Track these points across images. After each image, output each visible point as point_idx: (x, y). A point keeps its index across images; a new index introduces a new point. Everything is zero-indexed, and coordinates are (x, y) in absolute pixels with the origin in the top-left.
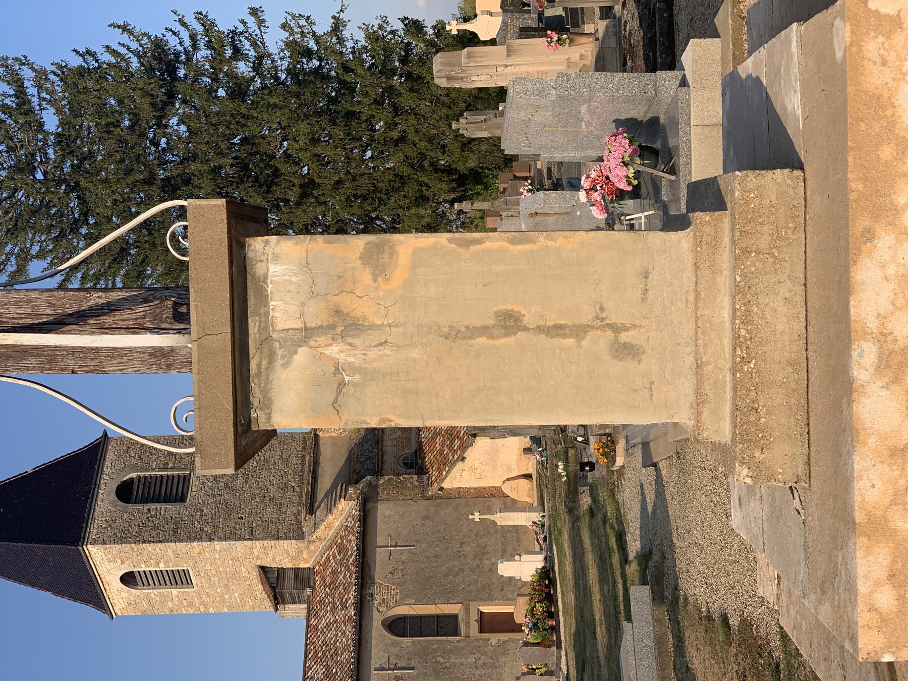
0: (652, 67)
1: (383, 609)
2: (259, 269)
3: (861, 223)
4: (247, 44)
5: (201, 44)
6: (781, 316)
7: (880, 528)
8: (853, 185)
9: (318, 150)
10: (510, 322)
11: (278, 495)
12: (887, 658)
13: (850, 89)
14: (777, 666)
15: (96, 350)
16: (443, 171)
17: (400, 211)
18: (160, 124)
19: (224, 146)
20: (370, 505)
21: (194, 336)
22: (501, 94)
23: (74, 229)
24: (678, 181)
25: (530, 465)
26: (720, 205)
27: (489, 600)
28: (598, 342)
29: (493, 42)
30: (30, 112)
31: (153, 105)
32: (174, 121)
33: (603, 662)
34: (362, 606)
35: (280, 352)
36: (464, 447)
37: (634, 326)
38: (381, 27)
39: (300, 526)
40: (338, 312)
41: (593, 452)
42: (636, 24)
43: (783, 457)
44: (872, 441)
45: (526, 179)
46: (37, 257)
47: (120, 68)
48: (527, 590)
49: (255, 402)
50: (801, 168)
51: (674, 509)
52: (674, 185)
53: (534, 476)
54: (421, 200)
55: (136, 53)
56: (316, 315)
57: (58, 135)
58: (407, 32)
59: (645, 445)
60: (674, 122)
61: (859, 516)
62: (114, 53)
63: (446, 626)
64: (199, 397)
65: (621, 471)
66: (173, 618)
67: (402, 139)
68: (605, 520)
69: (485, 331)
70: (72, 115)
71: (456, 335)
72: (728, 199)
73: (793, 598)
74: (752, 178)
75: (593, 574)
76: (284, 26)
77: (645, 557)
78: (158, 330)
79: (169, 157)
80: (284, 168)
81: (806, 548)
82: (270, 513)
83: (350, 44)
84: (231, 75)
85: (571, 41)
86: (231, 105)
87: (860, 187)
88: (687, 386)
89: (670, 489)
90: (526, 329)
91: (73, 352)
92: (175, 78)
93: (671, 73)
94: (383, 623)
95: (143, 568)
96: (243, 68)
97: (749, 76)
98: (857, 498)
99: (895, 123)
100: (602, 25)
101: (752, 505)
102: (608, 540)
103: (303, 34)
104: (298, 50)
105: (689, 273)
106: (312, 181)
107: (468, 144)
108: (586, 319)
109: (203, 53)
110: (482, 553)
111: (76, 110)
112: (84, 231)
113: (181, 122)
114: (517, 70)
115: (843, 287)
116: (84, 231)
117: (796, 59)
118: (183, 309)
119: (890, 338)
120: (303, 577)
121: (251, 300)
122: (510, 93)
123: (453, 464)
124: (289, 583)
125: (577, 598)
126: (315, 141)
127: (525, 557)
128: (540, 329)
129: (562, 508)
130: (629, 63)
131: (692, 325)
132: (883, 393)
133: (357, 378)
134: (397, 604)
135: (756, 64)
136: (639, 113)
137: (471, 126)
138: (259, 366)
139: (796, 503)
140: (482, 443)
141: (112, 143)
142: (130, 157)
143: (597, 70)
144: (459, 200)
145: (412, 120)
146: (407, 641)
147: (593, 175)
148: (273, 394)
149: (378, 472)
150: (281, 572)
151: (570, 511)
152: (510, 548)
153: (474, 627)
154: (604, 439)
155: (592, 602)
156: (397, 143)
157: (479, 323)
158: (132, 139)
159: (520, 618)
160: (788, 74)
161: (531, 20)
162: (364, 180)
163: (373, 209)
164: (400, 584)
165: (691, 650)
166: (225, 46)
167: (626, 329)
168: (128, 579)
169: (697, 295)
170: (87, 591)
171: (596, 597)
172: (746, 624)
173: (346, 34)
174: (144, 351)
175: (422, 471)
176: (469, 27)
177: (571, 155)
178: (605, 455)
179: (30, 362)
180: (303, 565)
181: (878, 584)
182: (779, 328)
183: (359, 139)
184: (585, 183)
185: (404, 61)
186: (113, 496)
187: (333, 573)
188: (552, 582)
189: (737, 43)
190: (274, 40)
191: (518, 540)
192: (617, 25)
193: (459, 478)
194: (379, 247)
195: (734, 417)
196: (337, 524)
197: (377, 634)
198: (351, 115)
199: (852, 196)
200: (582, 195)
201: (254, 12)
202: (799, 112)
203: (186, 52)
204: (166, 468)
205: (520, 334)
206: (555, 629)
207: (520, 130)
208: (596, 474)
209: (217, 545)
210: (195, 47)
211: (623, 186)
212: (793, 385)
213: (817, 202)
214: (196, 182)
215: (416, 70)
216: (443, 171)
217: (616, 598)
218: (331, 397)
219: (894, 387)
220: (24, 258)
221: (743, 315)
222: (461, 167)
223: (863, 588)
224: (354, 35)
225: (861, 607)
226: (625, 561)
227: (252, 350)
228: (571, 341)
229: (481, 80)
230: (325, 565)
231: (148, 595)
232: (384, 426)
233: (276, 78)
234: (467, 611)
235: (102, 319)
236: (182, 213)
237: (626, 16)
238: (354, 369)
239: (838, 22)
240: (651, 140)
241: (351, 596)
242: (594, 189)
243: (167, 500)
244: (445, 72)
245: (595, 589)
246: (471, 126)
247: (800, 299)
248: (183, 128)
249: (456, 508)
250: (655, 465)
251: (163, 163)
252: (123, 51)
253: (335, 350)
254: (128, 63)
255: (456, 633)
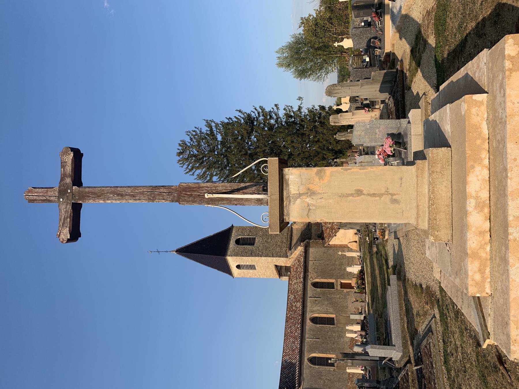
0: (398, 118)
1: (311, 279)
2: (287, 177)
3: (470, 163)
4: (274, 115)
5: (261, 115)
6: (444, 191)
7: (475, 256)
8: (467, 152)
9: (293, 144)
10: (359, 192)
11: (280, 244)
12: (478, 295)
13: (467, 123)
14: (438, 300)
15: (242, 199)
16: (330, 150)
17: (317, 162)
18: (249, 138)
19: (266, 144)
20: (307, 248)
21: (269, 195)
22: (351, 127)
23: (225, 168)
24: (407, 152)
25: (357, 238)
26: (424, 158)
27: (344, 278)
28: (387, 199)
29: (347, 112)
30: (214, 135)
31: (247, 133)
32: (253, 137)
33: (380, 298)
34: (305, 278)
35: (292, 200)
36: (336, 232)
37: (398, 194)
38: (312, 108)
39: (287, 254)
40: (309, 189)
41: (378, 234)
42: (393, 105)
43: (444, 234)
44: (473, 229)
45: (356, 152)
46: (215, 175)
47: (238, 122)
48: (356, 276)
49: (285, 214)
50: (450, 147)
51: (404, 252)
52: (406, 153)
53: (358, 242)
54: (324, 159)
55: (243, 118)
56: (302, 190)
57: (221, 141)
58: (320, 109)
59: (395, 232)
60: (406, 134)
61: (469, 252)
62: (237, 118)
63: (331, 286)
64: (270, 212)
65: (387, 241)
66: (250, 279)
67: (318, 141)
68: (381, 255)
69: (352, 195)
70: (225, 136)
71: (342, 196)
72: (427, 156)
73: (446, 277)
74: (435, 150)
75: (377, 272)
76: (284, 109)
77: (394, 267)
78: (259, 194)
79: (251, 147)
80: (283, 150)
81: (451, 262)
82: (278, 249)
83: (303, 114)
84: (269, 124)
85: (372, 111)
86: (269, 132)
87: (470, 152)
88: (414, 212)
89: (403, 246)
90: (364, 194)
91: (236, 199)
92: (253, 125)
93: (405, 120)
94: (311, 284)
95: (242, 264)
96: (272, 122)
97: (433, 120)
98: (468, 246)
99: (481, 133)
100: (382, 106)
101: (433, 249)
102: (382, 261)
103: (290, 111)
104: (288, 116)
105: (415, 178)
106: (291, 153)
107: (338, 142)
108: (383, 191)
109: (261, 118)
110: (341, 264)
111: (226, 134)
112: (228, 168)
113: (255, 137)
114: (355, 119)
115: (464, 182)
116: (228, 168)
117: (448, 115)
118: (265, 188)
119: (479, 198)
120: (288, 269)
121: (284, 186)
122: (355, 126)
123: (333, 237)
124: (283, 270)
125: (372, 279)
126: (292, 142)
127: (355, 266)
128: (369, 195)
129: (367, 252)
130: (391, 117)
131: (416, 194)
132: (477, 214)
133: (314, 208)
134: (315, 278)
135: (435, 117)
136: (395, 131)
137: (341, 137)
138: (286, 204)
139: (448, 248)
140: (341, 231)
141: (236, 144)
142: (240, 147)
143: (380, 119)
144: (336, 158)
145: (321, 135)
146: (319, 289)
147: (380, 150)
148: (290, 212)
149: (310, 239)
150: (281, 267)
151: (370, 253)
152: (350, 263)
153: (339, 287)
154: (381, 230)
155: (377, 280)
156: (316, 142)
157: (350, 193)
158: (241, 142)
159: (353, 285)
160: (446, 119)
161: (359, 105)
162: (307, 153)
163: (308, 161)
164: (316, 272)
165: (410, 295)
166: (267, 115)
167: (395, 195)
168: (238, 267)
169: (417, 185)
170: (227, 270)
171: (378, 279)
172: (428, 287)
173: (302, 111)
174: (254, 199)
175: (323, 239)
176: (339, 107)
177: (373, 144)
178: (382, 235)
179: (225, 202)
180: (287, 265)
181: (475, 272)
182: (443, 195)
183: (305, 141)
184: (377, 152)
185: (319, 118)
186: (234, 243)
187: (296, 268)
188: (364, 274)
189: (426, 110)
190: (281, 113)
191: (353, 261)
192: (387, 105)
193: (334, 241)
194: (321, 171)
195: (429, 222)
196: (298, 253)
197: (309, 287)
198: (303, 134)
199: (467, 155)
200: (376, 156)
201: (276, 105)
202: (449, 130)
203: (257, 118)
204: (249, 235)
205: (362, 196)
206: (365, 288)
207: (357, 138)
208: (379, 241)
209: (263, 258)
210: (259, 116)
211: (390, 153)
212: (447, 212)
213: (455, 157)
214: (258, 154)
215: (323, 121)
216: (330, 150)
217: (385, 279)
218: (306, 213)
219: (481, 213)
220: (212, 176)
221: (432, 191)
222: (336, 149)
223: (470, 273)
224: (305, 111)
225: (469, 279)
226: (388, 268)
227: (284, 200)
228: (378, 198)
229: (344, 123)
230: (294, 266)
231: (244, 272)
232: (322, 222)
233: (282, 124)
234: (337, 281)
235: (244, 191)
236: (266, 162)
237: (390, 103)
238: (314, 205)
239: (463, 103)
240: (399, 140)
241: (302, 275)
242: (380, 154)
243: (249, 244)
244: (333, 120)
245: (378, 276)
246: (341, 137)
247: (450, 186)
248: (255, 139)
249: (333, 250)
250: (398, 239)
251: (249, 149)
252: (239, 118)
253: (308, 200)
254: (241, 121)
255: (333, 288)
